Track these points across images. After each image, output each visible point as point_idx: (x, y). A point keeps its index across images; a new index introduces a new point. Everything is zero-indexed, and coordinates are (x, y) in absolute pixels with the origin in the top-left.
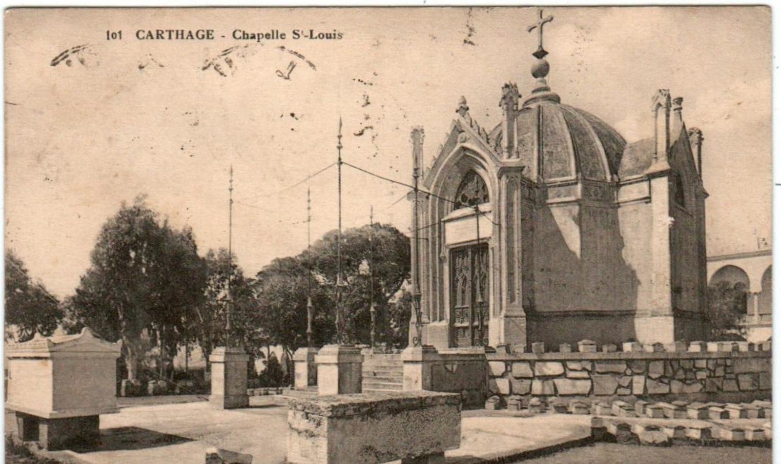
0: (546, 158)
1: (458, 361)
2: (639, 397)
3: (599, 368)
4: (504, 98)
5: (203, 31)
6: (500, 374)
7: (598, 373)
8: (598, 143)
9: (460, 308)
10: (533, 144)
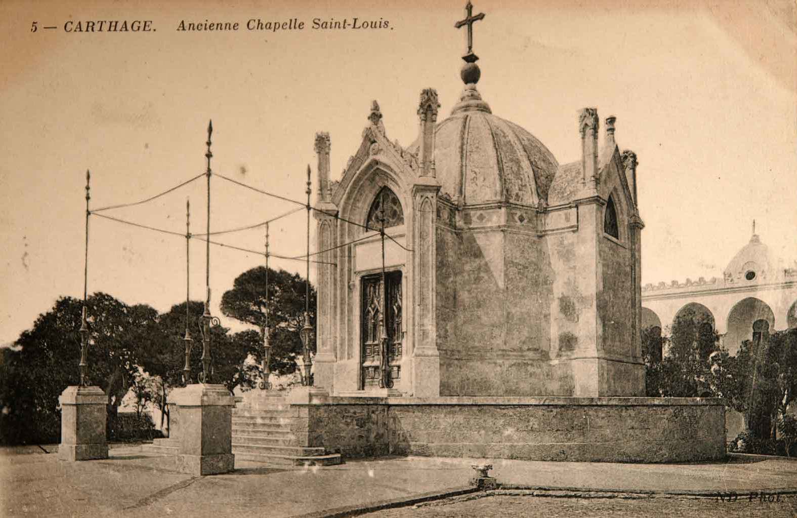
9: (370, 345)
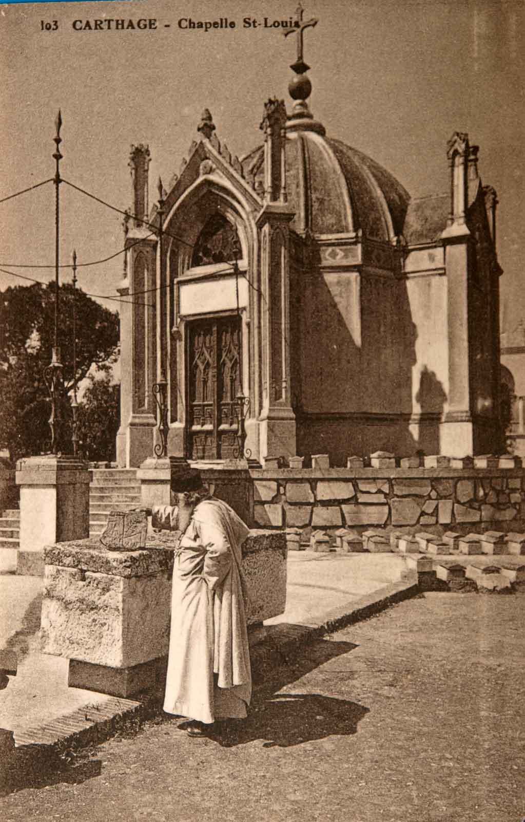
0: (316, 205)
1: (216, 480)
2: (447, 527)
3: (397, 490)
4: (269, 117)
5: (145, 20)
6: (270, 499)
7: (398, 496)
8: (379, 193)
9: (199, 405)
10: (298, 186)
